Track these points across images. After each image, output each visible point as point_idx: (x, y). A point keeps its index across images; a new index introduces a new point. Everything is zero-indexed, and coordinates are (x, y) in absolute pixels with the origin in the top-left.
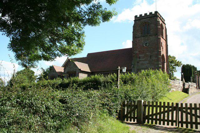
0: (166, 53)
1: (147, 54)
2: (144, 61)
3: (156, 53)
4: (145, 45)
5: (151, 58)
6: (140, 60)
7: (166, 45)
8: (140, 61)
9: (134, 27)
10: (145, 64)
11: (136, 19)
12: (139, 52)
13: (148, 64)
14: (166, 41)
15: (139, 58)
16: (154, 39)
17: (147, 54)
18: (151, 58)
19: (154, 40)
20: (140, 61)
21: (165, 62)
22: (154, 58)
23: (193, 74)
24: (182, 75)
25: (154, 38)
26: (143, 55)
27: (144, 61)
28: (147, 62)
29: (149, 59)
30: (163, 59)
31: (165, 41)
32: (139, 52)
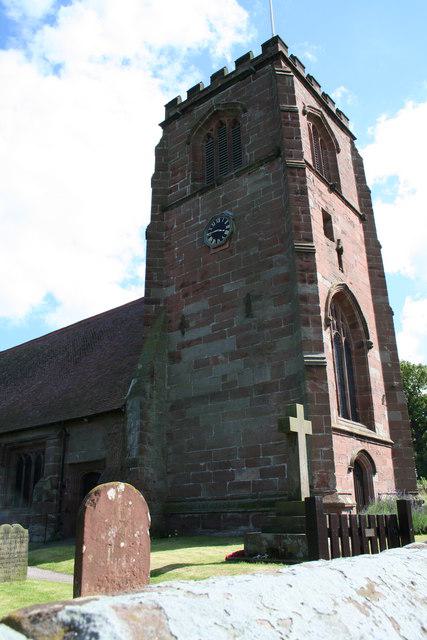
0: (374, 293)
1: (227, 288)
2: (209, 339)
3: (283, 270)
4: (216, 236)
5: (249, 313)
6: (190, 336)
7: (367, 243)
8: (189, 344)
9: (161, 152)
10: (216, 361)
11: (171, 114)
12: (182, 286)
13: (233, 356)
14: (362, 219)
15: (183, 326)
16: (265, 184)
17: (227, 288)
18: (249, 313)
19: (265, 190)
20: (189, 344)
21: (370, 346)
22: (268, 311)
23: (329, 121)
24: (238, 175)
25: (266, 178)
26: (203, 304)
27: (209, 339)
28: (230, 343)
29: (238, 320)
30: (354, 326)
31: (356, 220)
32: (182, 286)
